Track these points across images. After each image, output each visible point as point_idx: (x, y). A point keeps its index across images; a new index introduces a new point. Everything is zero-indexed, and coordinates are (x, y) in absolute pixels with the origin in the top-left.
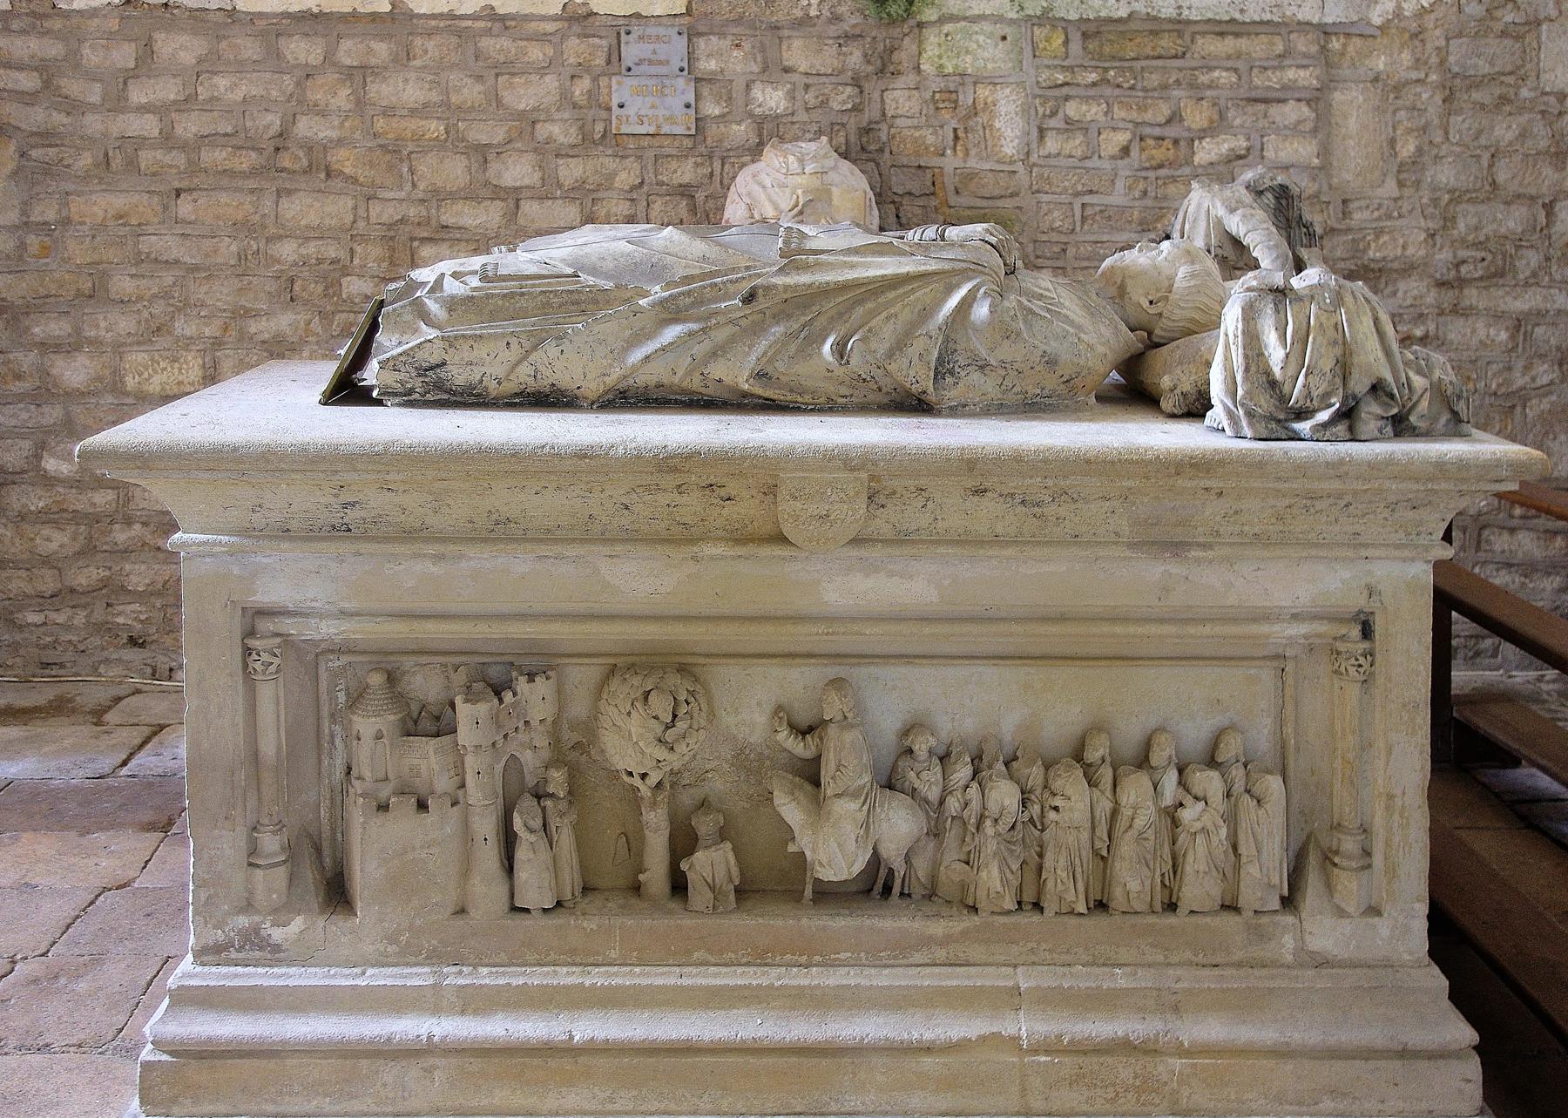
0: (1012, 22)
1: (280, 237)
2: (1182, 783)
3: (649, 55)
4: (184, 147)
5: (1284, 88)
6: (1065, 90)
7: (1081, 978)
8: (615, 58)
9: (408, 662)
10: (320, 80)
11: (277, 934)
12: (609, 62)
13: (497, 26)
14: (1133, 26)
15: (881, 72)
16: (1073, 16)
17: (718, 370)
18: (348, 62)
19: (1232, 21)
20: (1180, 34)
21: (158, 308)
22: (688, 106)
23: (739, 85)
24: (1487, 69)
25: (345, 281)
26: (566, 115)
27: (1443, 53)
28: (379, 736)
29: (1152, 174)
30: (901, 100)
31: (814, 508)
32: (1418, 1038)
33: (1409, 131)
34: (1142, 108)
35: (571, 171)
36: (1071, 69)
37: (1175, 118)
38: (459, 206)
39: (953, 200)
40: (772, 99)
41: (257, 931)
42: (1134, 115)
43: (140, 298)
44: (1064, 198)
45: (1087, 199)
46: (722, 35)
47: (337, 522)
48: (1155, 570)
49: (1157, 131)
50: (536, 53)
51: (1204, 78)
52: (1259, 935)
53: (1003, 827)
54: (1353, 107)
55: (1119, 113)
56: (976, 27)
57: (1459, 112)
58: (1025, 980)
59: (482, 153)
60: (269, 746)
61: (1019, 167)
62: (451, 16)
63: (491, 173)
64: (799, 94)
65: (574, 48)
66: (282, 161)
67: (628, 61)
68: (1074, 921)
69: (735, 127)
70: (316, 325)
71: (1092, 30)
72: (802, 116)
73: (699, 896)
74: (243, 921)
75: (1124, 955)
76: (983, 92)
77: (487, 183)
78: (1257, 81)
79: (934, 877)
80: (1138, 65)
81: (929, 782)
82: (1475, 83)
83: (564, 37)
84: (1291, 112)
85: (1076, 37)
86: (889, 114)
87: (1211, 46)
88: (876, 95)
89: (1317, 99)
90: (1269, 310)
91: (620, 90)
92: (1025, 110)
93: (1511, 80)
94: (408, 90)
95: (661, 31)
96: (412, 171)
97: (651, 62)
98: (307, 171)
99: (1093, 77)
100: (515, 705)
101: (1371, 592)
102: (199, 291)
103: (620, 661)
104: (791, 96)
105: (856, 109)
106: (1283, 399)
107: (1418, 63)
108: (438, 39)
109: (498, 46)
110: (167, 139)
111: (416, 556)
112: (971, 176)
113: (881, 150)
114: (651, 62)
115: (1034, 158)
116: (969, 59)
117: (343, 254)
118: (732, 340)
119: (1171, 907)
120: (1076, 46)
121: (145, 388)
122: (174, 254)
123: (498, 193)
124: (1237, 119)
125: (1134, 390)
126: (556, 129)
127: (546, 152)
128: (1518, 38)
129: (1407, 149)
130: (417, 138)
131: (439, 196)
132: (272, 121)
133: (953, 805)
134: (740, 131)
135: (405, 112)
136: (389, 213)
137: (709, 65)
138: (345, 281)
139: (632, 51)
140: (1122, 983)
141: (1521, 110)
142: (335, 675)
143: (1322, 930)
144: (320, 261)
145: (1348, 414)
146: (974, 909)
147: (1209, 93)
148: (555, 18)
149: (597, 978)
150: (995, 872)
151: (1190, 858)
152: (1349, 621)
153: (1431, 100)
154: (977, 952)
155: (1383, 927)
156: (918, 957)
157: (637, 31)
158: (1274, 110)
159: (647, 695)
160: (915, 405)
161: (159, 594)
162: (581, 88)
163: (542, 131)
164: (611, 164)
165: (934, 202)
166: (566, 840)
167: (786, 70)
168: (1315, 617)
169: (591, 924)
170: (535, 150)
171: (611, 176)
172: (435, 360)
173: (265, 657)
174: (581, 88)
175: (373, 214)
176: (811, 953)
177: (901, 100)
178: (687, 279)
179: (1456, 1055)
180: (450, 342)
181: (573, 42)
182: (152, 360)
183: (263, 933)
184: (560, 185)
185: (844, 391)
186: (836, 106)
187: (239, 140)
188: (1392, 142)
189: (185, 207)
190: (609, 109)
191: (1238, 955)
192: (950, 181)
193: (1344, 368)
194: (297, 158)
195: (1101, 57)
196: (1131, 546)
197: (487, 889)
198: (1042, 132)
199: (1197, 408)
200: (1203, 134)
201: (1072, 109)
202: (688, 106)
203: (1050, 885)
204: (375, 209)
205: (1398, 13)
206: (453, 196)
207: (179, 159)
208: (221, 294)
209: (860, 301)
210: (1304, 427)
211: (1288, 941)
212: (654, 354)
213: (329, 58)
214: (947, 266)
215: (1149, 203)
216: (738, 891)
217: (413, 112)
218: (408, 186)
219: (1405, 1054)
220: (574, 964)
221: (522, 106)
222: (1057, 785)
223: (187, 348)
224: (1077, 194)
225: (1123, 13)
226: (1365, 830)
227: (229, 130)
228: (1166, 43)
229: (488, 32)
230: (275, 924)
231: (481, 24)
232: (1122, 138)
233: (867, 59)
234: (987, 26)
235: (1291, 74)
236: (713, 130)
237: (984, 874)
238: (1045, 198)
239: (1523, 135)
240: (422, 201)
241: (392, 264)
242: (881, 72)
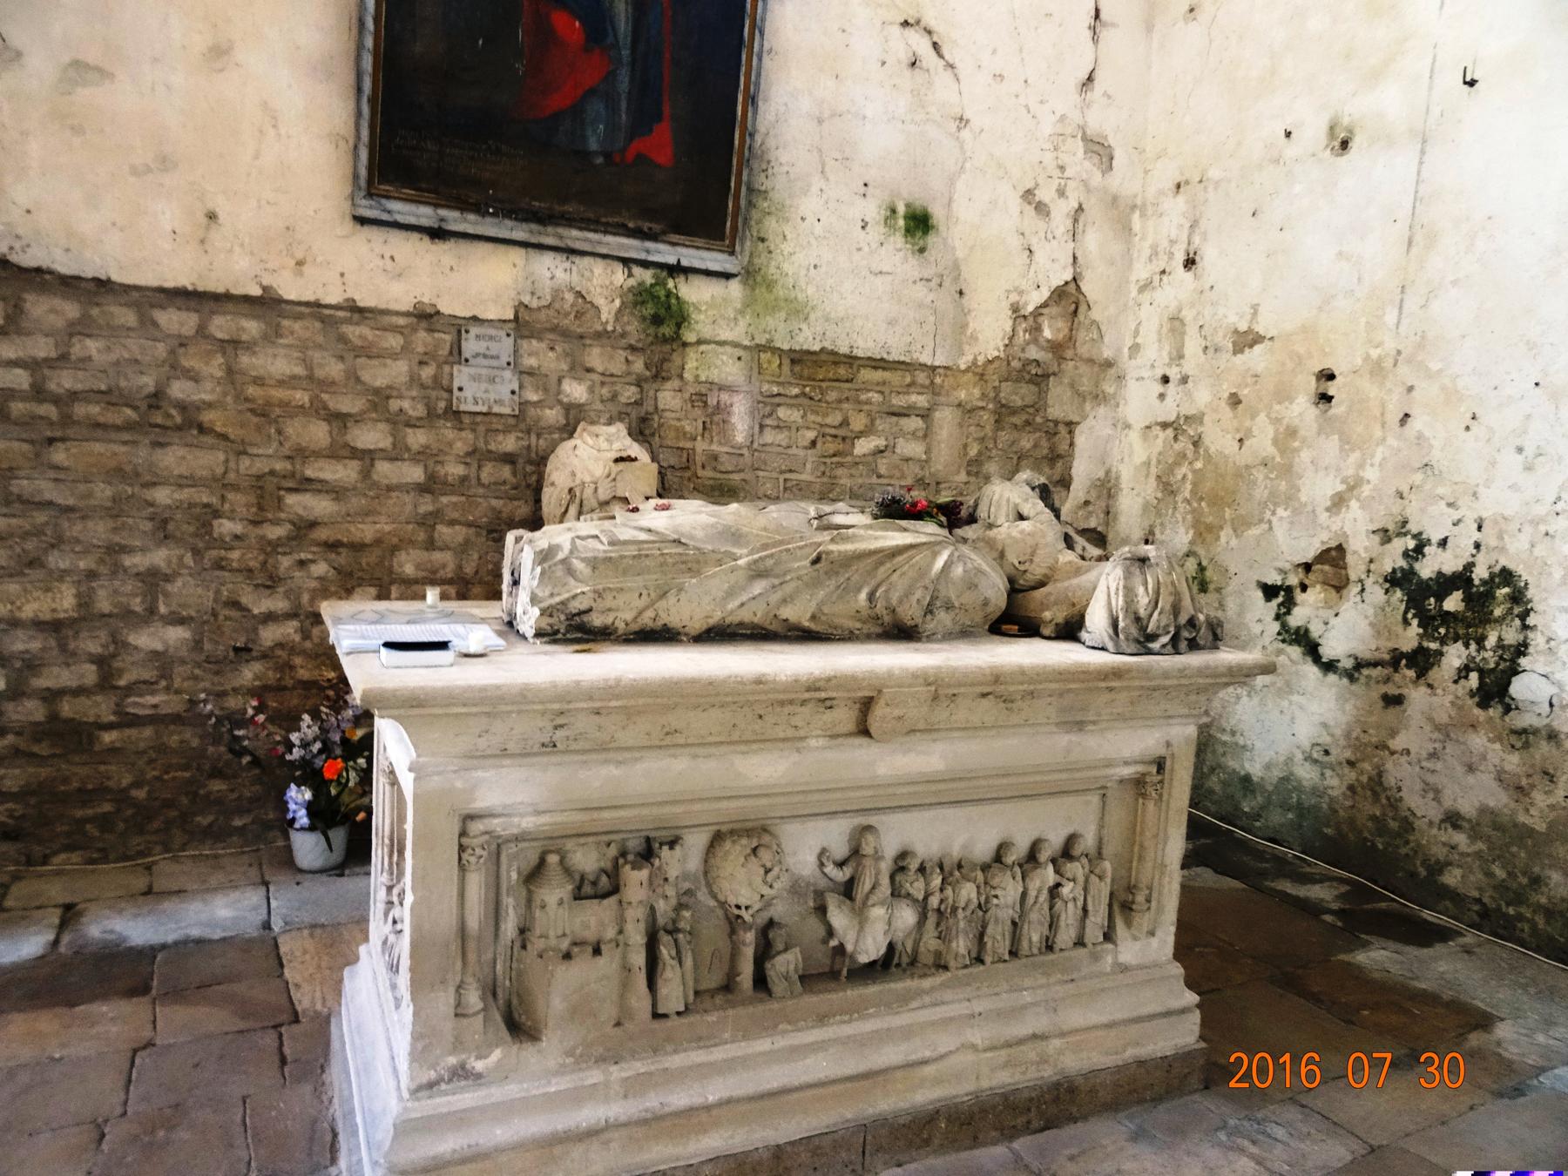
0: (745, 348)
1: (155, 484)
2: (1057, 872)
3: (482, 351)
4: (56, 400)
5: (909, 407)
6: (777, 400)
7: (1006, 1000)
8: (455, 352)
9: (569, 844)
10: (192, 350)
11: (479, 1066)
12: (451, 353)
13: (356, 316)
14: (823, 357)
15: (655, 377)
16: (786, 347)
17: (788, 613)
18: (220, 335)
19: (882, 359)
20: (851, 365)
21: (30, 545)
22: (513, 392)
23: (553, 379)
24: (1019, 403)
25: (216, 523)
26: (414, 393)
27: (997, 389)
28: (561, 902)
29: (828, 460)
30: (668, 398)
31: (897, 712)
32: (1176, 1004)
33: (975, 439)
34: (826, 415)
35: (417, 438)
36: (779, 384)
37: (845, 423)
38: (321, 463)
39: (700, 473)
40: (576, 391)
41: (463, 1066)
42: (819, 419)
43: (12, 535)
44: (775, 475)
45: (788, 476)
46: (540, 339)
47: (546, 740)
48: (1064, 739)
49: (833, 431)
50: (394, 341)
51: (863, 397)
52: (1096, 957)
53: (968, 912)
54: (945, 418)
55: (811, 417)
56: (721, 350)
57: (1003, 429)
58: (978, 1006)
59: (339, 420)
60: (473, 923)
61: (745, 451)
62: (317, 304)
63: (349, 438)
64: (597, 390)
65: (422, 339)
66: (160, 418)
67: (466, 353)
68: (1001, 965)
69: (548, 411)
70: (189, 559)
71: (799, 359)
72: (599, 406)
73: (778, 987)
74: (452, 1060)
75: (1027, 982)
76: (724, 397)
77: (346, 445)
78: (894, 401)
79: (916, 951)
80: (824, 385)
81: (917, 888)
82: (1014, 412)
83: (415, 330)
84: (914, 423)
85: (786, 362)
86: (661, 406)
87: (867, 375)
88: (651, 393)
89: (926, 415)
90: (1137, 572)
91: (461, 376)
92: (752, 413)
93: (1031, 410)
94: (277, 363)
95: (492, 332)
96: (279, 432)
97: (485, 356)
98: (179, 428)
99: (796, 391)
100: (659, 868)
101: (1168, 744)
102: (74, 529)
103: (724, 828)
104: (591, 390)
105: (638, 403)
106: (1143, 629)
107: (984, 396)
108: (306, 323)
109: (355, 332)
110: (38, 393)
111: (606, 762)
112: (715, 457)
113: (653, 435)
114: (485, 356)
115: (755, 445)
116: (716, 372)
117: (214, 500)
118: (797, 591)
119: (1050, 948)
120: (786, 368)
121: (17, 614)
122: (47, 496)
123: (356, 453)
124: (881, 425)
125: (1014, 620)
126: (406, 404)
127: (399, 422)
128: (1037, 384)
129: (973, 451)
130: (284, 404)
131: (301, 454)
132: (148, 382)
133: (934, 901)
134: (552, 415)
135: (272, 382)
136: (261, 466)
137: (531, 362)
138: (216, 523)
139: (470, 346)
140: (1029, 999)
141: (1037, 430)
142: (515, 856)
143: (1129, 950)
144: (191, 505)
145: (1175, 640)
146: (946, 968)
147: (866, 407)
148: (407, 314)
149: (718, 1054)
150: (961, 943)
151: (1063, 917)
152: (1151, 763)
153: (986, 417)
154: (948, 995)
155: (1154, 942)
156: (914, 1004)
157: (474, 330)
158: (904, 421)
159: (754, 850)
160: (901, 632)
161: (33, 793)
162: (427, 373)
163: (394, 405)
164: (450, 434)
165: (687, 474)
166: (689, 962)
167: (589, 370)
168: (1136, 762)
169: (712, 1018)
170: (387, 420)
171: (450, 445)
172: (583, 607)
173: (479, 851)
174: (427, 373)
175: (242, 467)
176: (855, 1011)
177: (668, 398)
178: (765, 547)
179: (1183, 1011)
180: (599, 594)
181: (422, 334)
182: (25, 590)
183: (468, 1066)
184: (408, 449)
185: (858, 625)
186: (623, 400)
187: (111, 397)
188: (965, 446)
189: (59, 455)
190: (450, 391)
191: (1085, 971)
192: (699, 459)
193: (1176, 610)
194: (169, 416)
195: (801, 377)
196: (1057, 724)
197: (640, 1000)
198: (762, 427)
199: (1070, 630)
200: (860, 434)
201: (782, 413)
202: (513, 392)
203: (989, 945)
204: (245, 462)
205: (975, 362)
206: (317, 454)
207: (49, 410)
208: (99, 530)
209: (882, 563)
210: (1155, 646)
211: (1109, 959)
212: (750, 604)
213: (202, 331)
214: (932, 539)
215: (825, 480)
216: (802, 978)
217: (281, 383)
218: (275, 445)
219: (1168, 1014)
220: (700, 1048)
221: (378, 383)
222: (995, 882)
223: (61, 579)
224: (782, 472)
225: (816, 348)
226: (1150, 888)
227: (103, 387)
228: (842, 371)
229: (349, 321)
230: (479, 1058)
231: (341, 314)
232: (811, 435)
233: (647, 366)
234: (728, 349)
235: (914, 398)
236: (532, 412)
237: (954, 944)
238: (761, 474)
239: (1035, 446)
240: (289, 457)
241: (261, 508)
242: (655, 377)
